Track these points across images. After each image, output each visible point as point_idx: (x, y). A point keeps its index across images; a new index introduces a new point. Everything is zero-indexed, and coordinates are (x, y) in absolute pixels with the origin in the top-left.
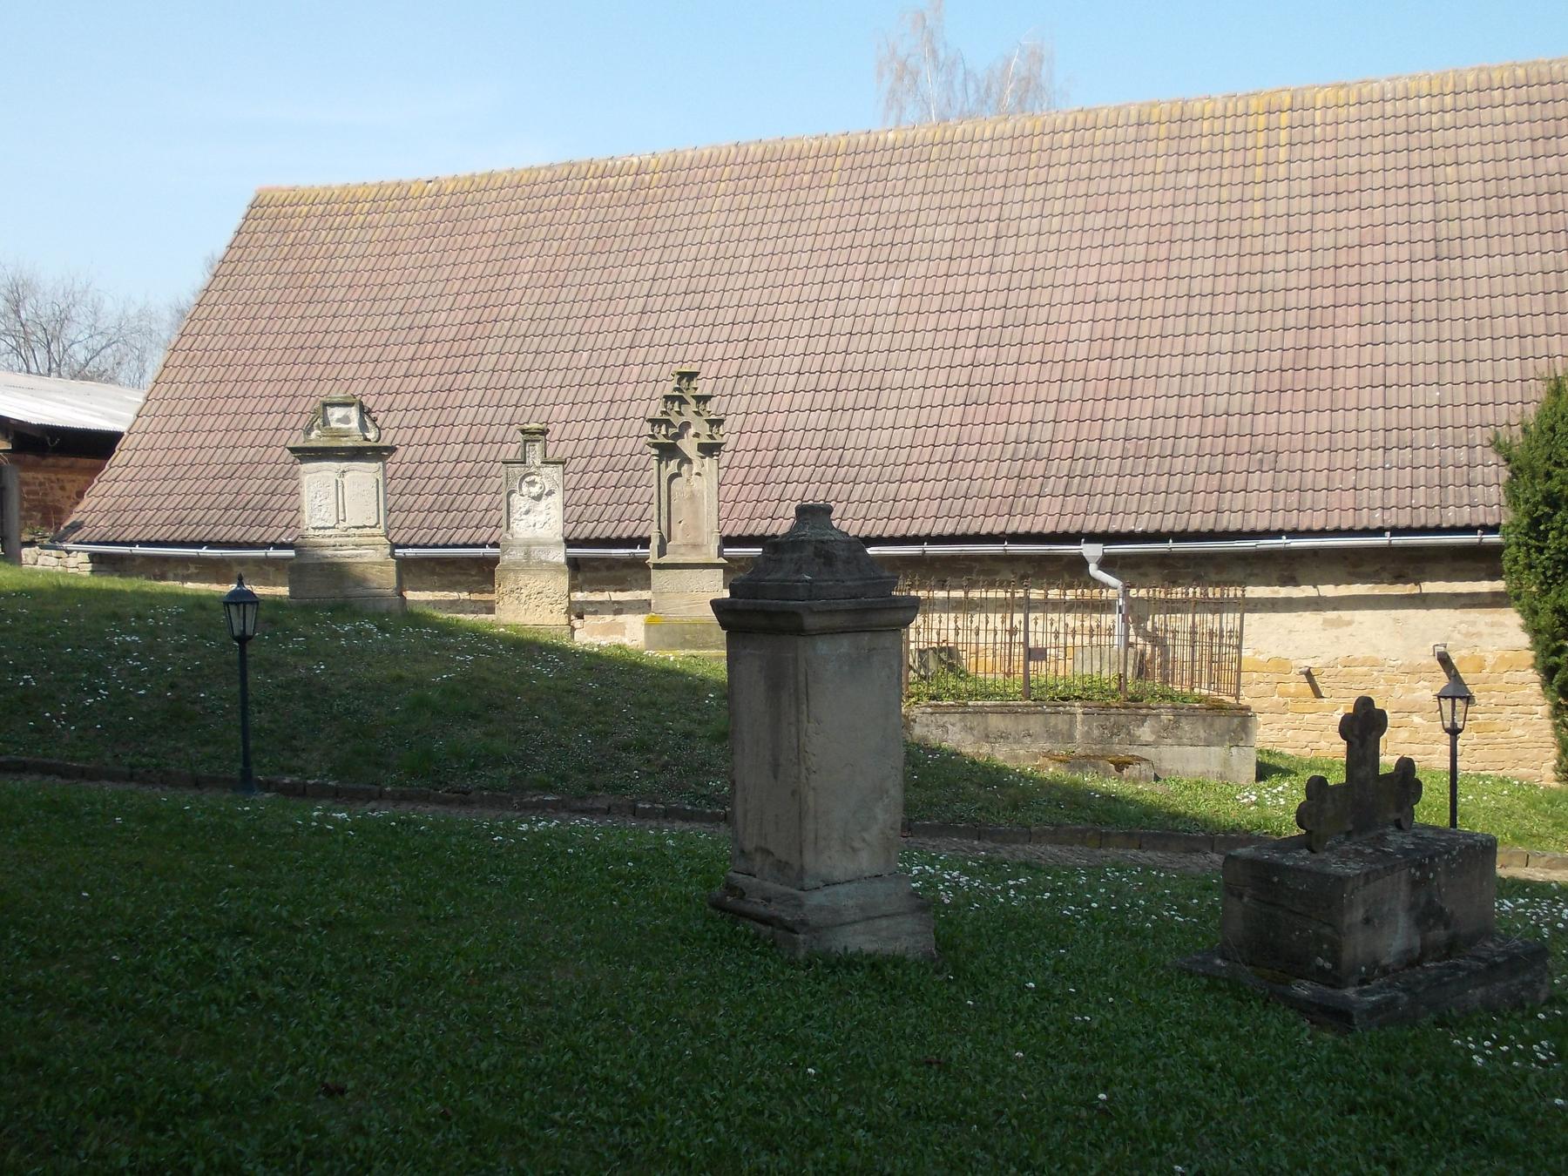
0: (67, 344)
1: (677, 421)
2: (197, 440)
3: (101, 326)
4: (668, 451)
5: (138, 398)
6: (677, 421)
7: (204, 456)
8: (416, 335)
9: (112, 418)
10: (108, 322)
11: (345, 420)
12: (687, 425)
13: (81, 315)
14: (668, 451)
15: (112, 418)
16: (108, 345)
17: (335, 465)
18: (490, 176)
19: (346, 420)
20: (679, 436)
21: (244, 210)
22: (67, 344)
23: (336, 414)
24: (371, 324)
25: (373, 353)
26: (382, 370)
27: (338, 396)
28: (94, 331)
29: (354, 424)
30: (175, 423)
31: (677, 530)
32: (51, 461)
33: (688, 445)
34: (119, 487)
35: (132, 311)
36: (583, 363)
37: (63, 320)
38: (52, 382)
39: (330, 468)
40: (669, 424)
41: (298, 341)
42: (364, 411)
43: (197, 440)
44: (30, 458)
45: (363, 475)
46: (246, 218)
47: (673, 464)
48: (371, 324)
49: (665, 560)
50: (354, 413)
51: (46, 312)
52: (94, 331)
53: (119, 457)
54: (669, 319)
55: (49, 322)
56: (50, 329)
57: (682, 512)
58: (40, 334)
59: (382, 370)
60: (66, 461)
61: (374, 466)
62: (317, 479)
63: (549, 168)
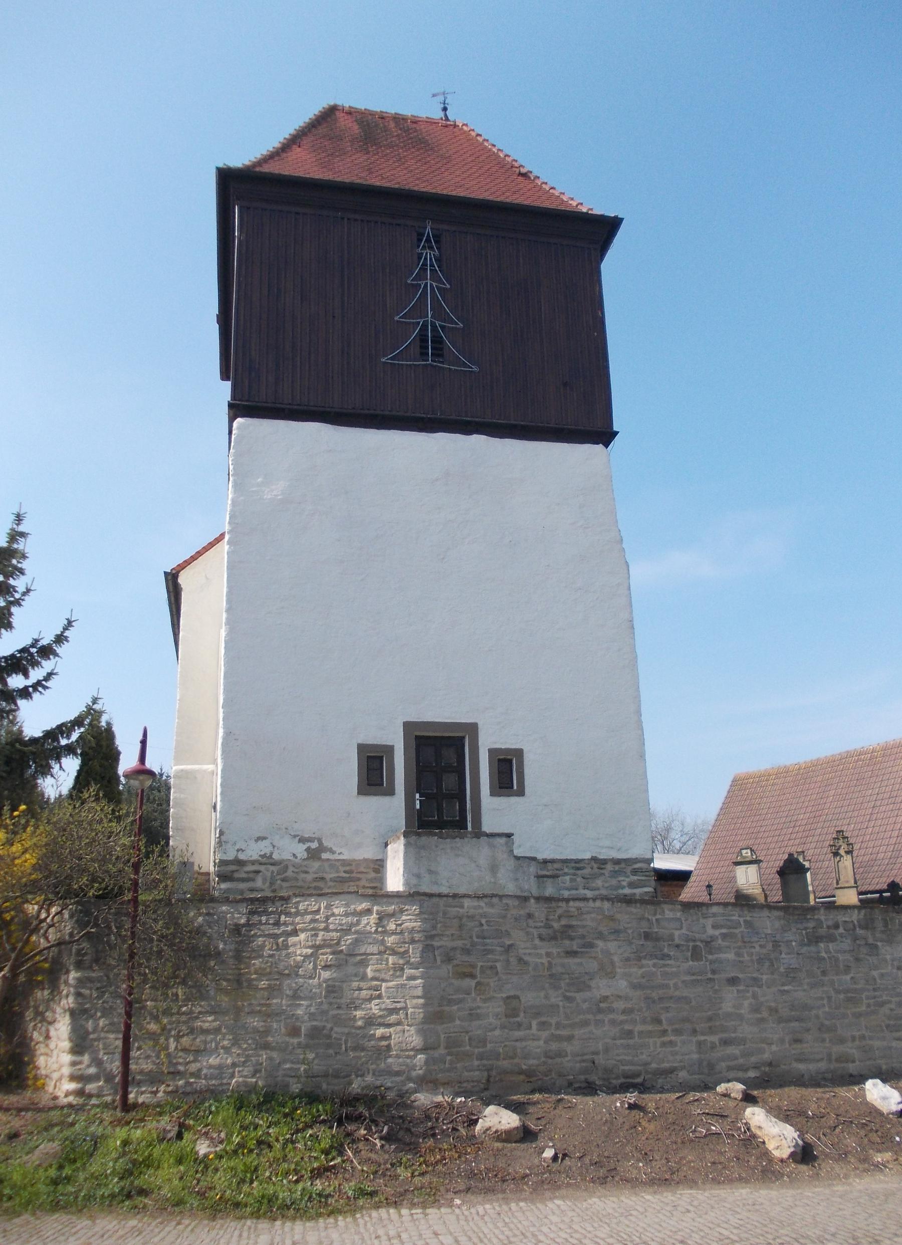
0: (671, 840)
1: (838, 845)
2: (718, 870)
3: (686, 830)
4: (836, 854)
5: (696, 858)
6: (838, 845)
7: (721, 875)
8: (792, 824)
9: (690, 866)
10: (688, 828)
11: (747, 853)
12: (841, 846)
13: (676, 826)
14: (836, 854)
15: (690, 866)
16: (689, 840)
17: (745, 866)
18: (818, 760)
19: (747, 853)
20: (838, 849)
21: (730, 783)
22: (671, 840)
23: (744, 852)
24: (777, 821)
25: (777, 833)
26: (781, 838)
27: (744, 847)
28: (683, 833)
29: (750, 854)
30: (710, 865)
31: (841, 877)
32: (669, 883)
33: (842, 852)
34: (693, 890)
35: (699, 821)
36: (852, 829)
37: (668, 829)
38: (666, 856)
39: (743, 867)
40: (835, 846)
41: (751, 830)
42: (752, 850)
43: (718, 870)
44: (662, 882)
45: (753, 869)
46: (731, 786)
47: (838, 858)
48: (777, 821)
49: (839, 886)
50: (749, 851)
51: (661, 826)
52: (683, 833)
53: (692, 879)
54: (883, 809)
55: (662, 831)
56: (663, 834)
57: (842, 872)
58: (659, 837)
59: (781, 838)
60: (675, 883)
61: (756, 865)
62: (740, 871)
63: (839, 755)
